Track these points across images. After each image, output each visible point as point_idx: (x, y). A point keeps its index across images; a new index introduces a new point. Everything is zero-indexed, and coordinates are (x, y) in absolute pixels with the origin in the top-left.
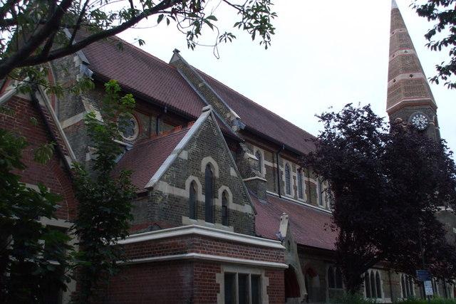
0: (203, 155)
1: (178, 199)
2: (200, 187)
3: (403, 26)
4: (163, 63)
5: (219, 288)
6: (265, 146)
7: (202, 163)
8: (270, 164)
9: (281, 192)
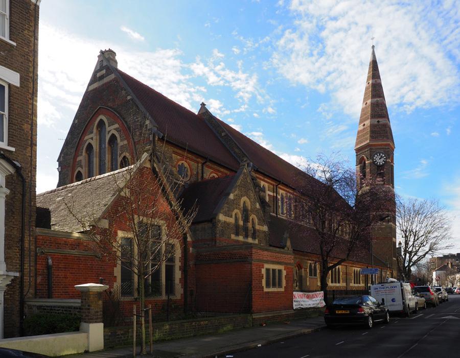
0: (242, 196)
1: (228, 224)
2: (240, 216)
3: (379, 77)
4: (193, 114)
5: (263, 276)
6: (268, 181)
7: (242, 200)
8: (271, 194)
9: (278, 213)
